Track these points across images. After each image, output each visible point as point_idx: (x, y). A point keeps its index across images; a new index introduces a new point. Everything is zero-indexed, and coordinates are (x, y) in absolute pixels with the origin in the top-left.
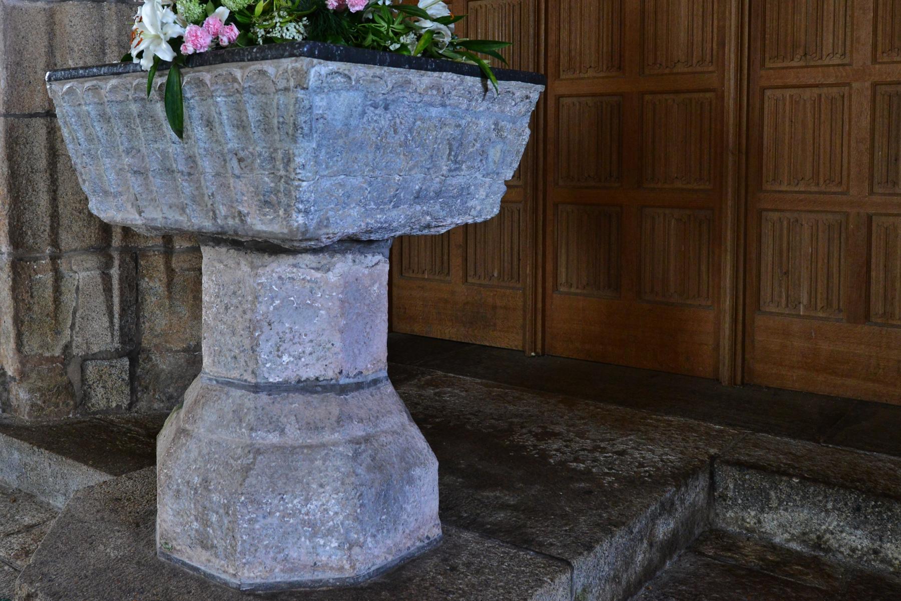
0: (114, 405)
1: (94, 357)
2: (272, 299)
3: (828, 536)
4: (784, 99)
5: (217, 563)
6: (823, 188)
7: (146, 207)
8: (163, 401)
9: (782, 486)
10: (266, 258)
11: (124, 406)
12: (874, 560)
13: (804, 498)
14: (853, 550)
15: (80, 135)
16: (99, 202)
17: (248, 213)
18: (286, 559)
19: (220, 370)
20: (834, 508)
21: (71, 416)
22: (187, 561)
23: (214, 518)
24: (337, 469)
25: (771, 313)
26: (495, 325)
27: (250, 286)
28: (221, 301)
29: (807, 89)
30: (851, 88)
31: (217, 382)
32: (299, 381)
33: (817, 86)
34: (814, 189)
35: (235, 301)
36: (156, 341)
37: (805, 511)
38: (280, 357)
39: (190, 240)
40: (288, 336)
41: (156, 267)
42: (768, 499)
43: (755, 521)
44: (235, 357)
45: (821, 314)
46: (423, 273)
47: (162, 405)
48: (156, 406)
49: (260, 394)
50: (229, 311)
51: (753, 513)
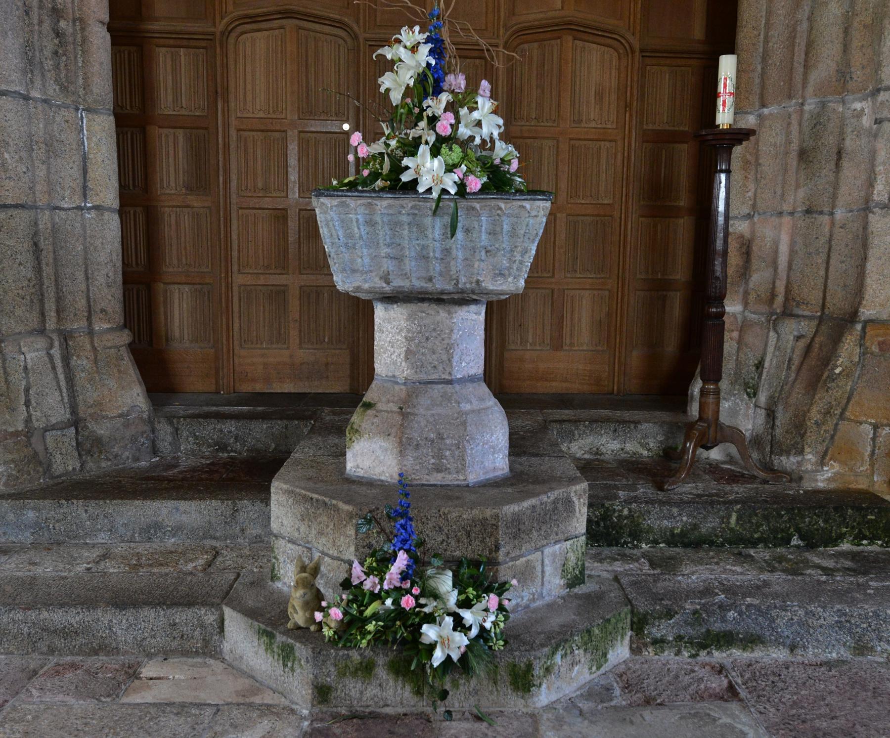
0: (70, 468)
1: (53, 427)
2: (459, 331)
5: (450, 477)
6: (540, 274)
8: (110, 460)
9: (581, 427)
10: (457, 308)
11: (78, 468)
13: (591, 431)
14: (613, 451)
15: (341, 234)
16: (345, 277)
18: (484, 468)
20: (605, 432)
21: (41, 481)
23: (448, 453)
25: (512, 350)
26: (327, 377)
31: (420, 383)
34: (536, 275)
35: (434, 334)
36: (90, 411)
39: (109, 322)
41: (82, 346)
42: (574, 435)
44: (435, 367)
45: (538, 348)
46: (262, 343)
47: (109, 463)
48: (103, 465)
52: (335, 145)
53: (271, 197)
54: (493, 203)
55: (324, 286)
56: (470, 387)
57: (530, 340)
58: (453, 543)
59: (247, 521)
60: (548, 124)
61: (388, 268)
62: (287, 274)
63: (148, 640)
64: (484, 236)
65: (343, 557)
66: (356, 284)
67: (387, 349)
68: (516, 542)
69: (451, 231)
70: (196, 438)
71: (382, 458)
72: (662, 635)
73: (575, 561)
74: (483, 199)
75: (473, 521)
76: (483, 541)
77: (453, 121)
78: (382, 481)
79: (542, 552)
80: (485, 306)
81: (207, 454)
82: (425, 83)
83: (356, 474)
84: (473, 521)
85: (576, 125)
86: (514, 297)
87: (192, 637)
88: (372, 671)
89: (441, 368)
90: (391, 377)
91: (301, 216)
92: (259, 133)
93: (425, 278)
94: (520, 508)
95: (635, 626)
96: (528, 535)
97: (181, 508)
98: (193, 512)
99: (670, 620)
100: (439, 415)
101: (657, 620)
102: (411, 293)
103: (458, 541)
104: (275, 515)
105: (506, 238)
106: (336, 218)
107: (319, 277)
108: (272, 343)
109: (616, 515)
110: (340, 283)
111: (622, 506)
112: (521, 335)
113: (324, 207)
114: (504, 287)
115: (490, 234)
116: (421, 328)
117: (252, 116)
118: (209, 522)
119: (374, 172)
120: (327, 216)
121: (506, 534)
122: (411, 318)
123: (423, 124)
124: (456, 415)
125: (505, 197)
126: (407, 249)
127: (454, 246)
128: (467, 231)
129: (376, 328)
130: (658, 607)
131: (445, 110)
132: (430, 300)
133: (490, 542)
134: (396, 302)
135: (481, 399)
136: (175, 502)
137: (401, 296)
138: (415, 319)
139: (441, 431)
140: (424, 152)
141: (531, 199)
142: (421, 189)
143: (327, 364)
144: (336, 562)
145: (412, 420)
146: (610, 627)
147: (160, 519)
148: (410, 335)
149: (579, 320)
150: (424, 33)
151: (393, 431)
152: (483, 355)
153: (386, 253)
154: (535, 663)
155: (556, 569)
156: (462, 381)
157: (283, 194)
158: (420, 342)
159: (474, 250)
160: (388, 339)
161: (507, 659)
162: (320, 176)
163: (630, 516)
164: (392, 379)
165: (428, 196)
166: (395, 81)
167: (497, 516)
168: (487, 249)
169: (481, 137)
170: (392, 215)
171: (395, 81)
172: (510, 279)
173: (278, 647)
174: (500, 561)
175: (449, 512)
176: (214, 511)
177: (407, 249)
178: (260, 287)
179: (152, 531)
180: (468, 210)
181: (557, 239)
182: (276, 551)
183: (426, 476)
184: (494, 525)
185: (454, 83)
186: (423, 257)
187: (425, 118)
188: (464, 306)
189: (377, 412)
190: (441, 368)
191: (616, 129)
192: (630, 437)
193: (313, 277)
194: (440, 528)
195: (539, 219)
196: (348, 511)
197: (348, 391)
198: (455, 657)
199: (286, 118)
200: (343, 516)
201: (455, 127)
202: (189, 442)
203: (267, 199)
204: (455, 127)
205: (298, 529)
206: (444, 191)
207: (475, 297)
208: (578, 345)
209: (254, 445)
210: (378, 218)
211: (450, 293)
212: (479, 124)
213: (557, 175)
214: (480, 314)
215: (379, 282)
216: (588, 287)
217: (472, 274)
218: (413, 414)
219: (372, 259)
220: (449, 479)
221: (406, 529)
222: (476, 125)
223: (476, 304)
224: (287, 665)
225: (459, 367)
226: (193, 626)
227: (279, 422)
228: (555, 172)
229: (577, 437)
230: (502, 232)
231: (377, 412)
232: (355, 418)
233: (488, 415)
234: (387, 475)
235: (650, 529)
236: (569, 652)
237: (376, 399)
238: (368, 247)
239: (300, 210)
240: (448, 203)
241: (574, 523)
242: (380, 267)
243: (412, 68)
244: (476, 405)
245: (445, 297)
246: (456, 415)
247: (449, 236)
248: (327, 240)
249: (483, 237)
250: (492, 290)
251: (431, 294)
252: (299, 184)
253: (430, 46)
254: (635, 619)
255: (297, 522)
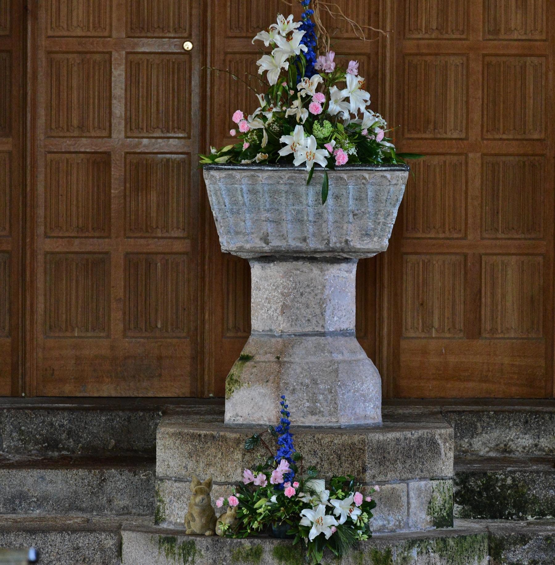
2: (331, 287)
3: (510, 443)
4: (419, 164)
5: (323, 419)
6: (447, 234)
7: (273, 240)
9: (485, 418)
12: (535, 451)
13: (497, 423)
14: (524, 448)
15: (227, 201)
17: (352, 240)
19: (297, 329)
22: (301, 425)
23: (321, 397)
24: (369, 370)
25: (412, 338)
26: (160, 375)
27: (319, 281)
28: (297, 291)
29: (437, 157)
30: (467, 157)
31: (295, 335)
32: (341, 331)
33: (443, 154)
34: (441, 235)
35: (308, 290)
37: (498, 431)
38: (333, 317)
40: (337, 306)
42: (476, 428)
43: (468, 445)
44: (309, 320)
45: (447, 335)
46: (73, 330)
49: (327, 337)
50: (304, 296)
51: (466, 440)
52: (173, 69)
53: (91, 137)
54: (359, 174)
55: (157, 253)
56: (342, 341)
57: (436, 325)
58: (326, 466)
59: (115, 491)
60: (454, 36)
61: (267, 230)
62: (109, 237)
63: (54, 563)
64: (351, 202)
65: (230, 481)
66: (239, 244)
67: (263, 306)
68: (382, 468)
69: (322, 197)
70: (21, 433)
71: (261, 403)
72: (518, 560)
73: (442, 502)
74: (349, 170)
75: (343, 445)
76: (352, 463)
77: (324, 100)
78: (261, 425)
79: (408, 485)
80: (354, 268)
81: (33, 452)
82: (299, 63)
83: (236, 422)
84: (343, 445)
85: (491, 37)
86: (381, 255)
87: (93, 560)
88: (260, 556)
89: (314, 322)
90: (268, 331)
91: (128, 161)
92: (75, 55)
93: (300, 239)
94: (385, 438)
95: (492, 551)
96: (393, 464)
97: (47, 478)
98: (59, 482)
99: (524, 545)
100: (312, 363)
101: (512, 546)
102: (288, 252)
103: (331, 464)
104: (161, 459)
105: (370, 203)
106: (223, 188)
107: (150, 241)
108: (87, 331)
109: (499, 484)
110: (225, 244)
111: (505, 475)
112: (423, 319)
113: (213, 179)
114: (370, 246)
115: (356, 200)
116: (296, 285)
117: (65, 33)
118: (75, 492)
119: (254, 145)
120: (216, 186)
121: (372, 458)
122: (287, 275)
123: (297, 103)
124: (328, 363)
125: (369, 168)
126: (284, 214)
127: (325, 211)
128: (337, 197)
129: (253, 286)
130: (513, 534)
131: (317, 90)
132: (304, 259)
133: (358, 464)
134: (273, 261)
135: (353, 352)
136: (42, 471)
137: (277, 255)
138: (290, 276)
139: (315, 377)
140: (299, 131)
141: (391, 170)
142: (297, 163)
143: (160, 358)
144: (223, 487)
145: (289, 368)
146: (466, 545)
147: (25, 489)
148: (286, 291)
149: (504, 296)
150: (298, 21)
151: (271, 378)
152: (355, 311)
153: (266, 217)
154: (393, 550)
155: (422, 504)
156: (334, 334)
157: (105, 134)
158: (295, 297)
159: (343, 213)
160: (265, 296)
161: (370, 546)
162: (154, 109)
163: (514, 486)
164: (269, 333)
165: (303, 169)
166: (272, 62)
167: (363, 441)
168: (355, 213)
169: (349, 111)
170: (271, 184)
171: (272, 62)
172: (375, 239)
173: (179, 548)
174: (367, 481)
175: (322, 438)
176: (81, 481)
177: (284, 214)
178: (72, 256)
179: (17, 502)
180: (337, 180)
181: (470, 188)
182: (161, 494)
183: (302, 419)
184: (361, 449)
185: (325, 64)
186: (299, 221)
187: (300, 98)
188: (335, 264)
189: (255, 363)
190: (314, 322)
191: (545, 41)
192: (544, 430)
193: (142, 241)
194: (315, 452)
195: (398, 186)
196: (235, 438)
197: (189, 396)
198: (328, 535)
199: (110, 37)
200: (231, 444)
201: (325, 106)
202: (12, 439)
203: (84, 140)
204: (325, 106)
205: (186, 467)
206: (316, 165)
207: (345, 255)
208: (502, 332)
209: (90, 442)
210: (259, 188)
211: (322, 252)
212: (347, 100)
213: (467, 102)
214: (351, 272)
215: (260, 242)
216: (513, 251)
217: (342, 235)
218: (288, 362)
219: (253, 223)
220: (323, 421)
221: (287, 442)
222: (344, 101)
223: (347, 262)
224: (188, 560)
225: (331, 321)
226: (94, 550)
227: (121, 413)
228: (465, 99)
229: (480, 430)
230: (367, 198)
231: (255, 363)
232: (234, 371)
233: (359, 366)
234: (266, 419)
235: (535, 500)
236: (424, 551)
237: (254, 352)
238: (250, 212)
239: (127, 153)
240: (319, 174)
241: (440, 465)
242: (260, 229)
243: (287, 53)
244: (347, 356)
245: (317, 256)
246: (328, 363)
247: (321, 202)
248: (215, 207)
249: (351, 203)
250: (360, 249)
251: (304, 252)
252: (126, 120)
253: (303, 32)
254: (493, 545)
255: (184, 460)
